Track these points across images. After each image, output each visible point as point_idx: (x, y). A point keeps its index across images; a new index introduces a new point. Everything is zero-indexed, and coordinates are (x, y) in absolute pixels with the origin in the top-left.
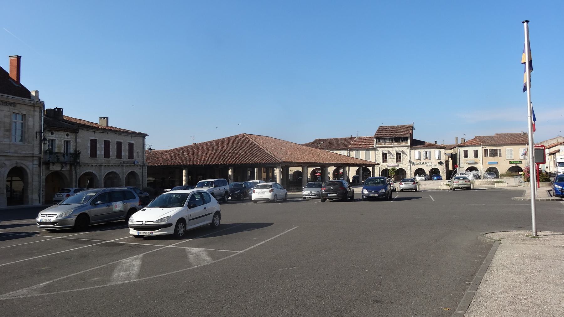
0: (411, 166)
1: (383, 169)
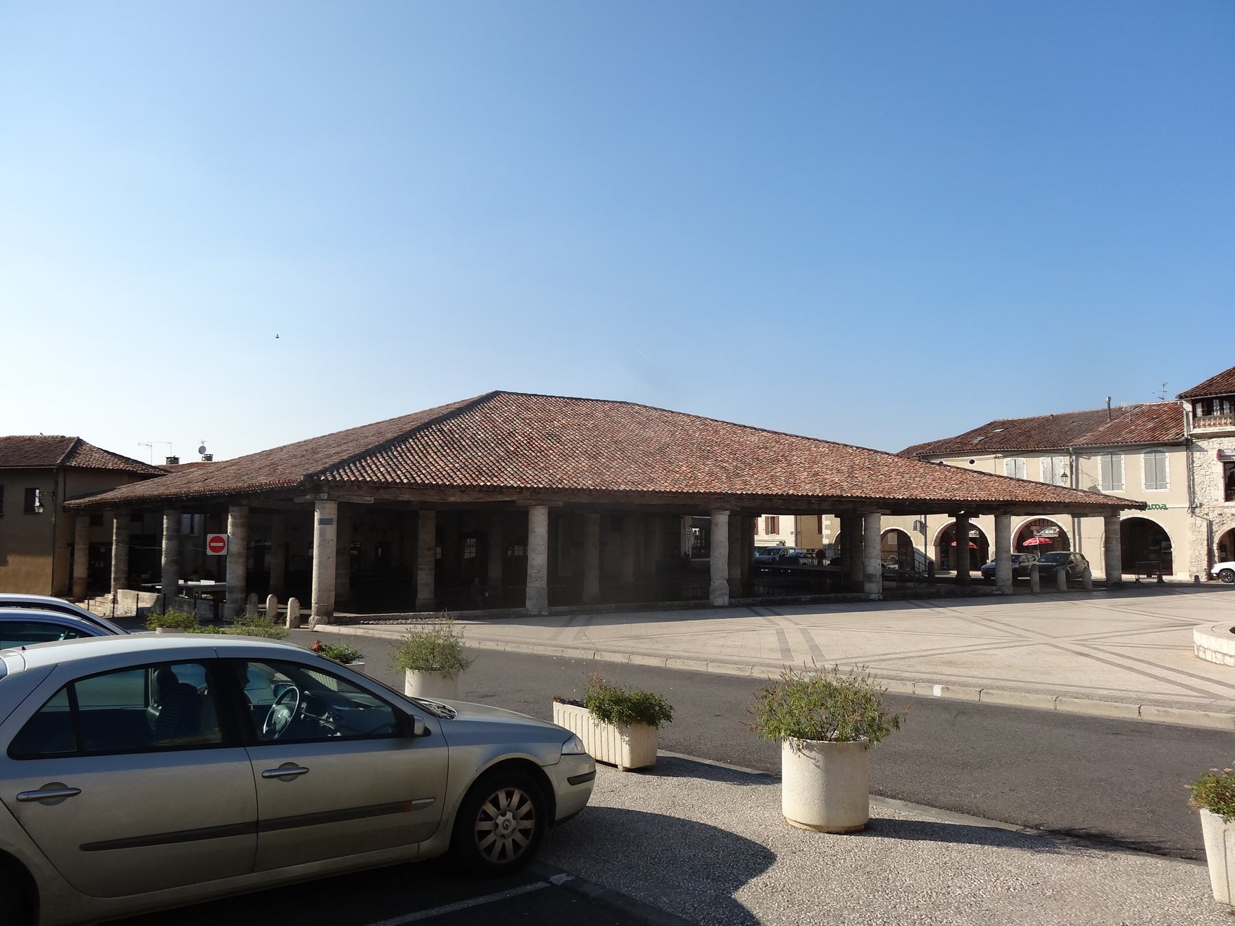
1: (1226, 528)
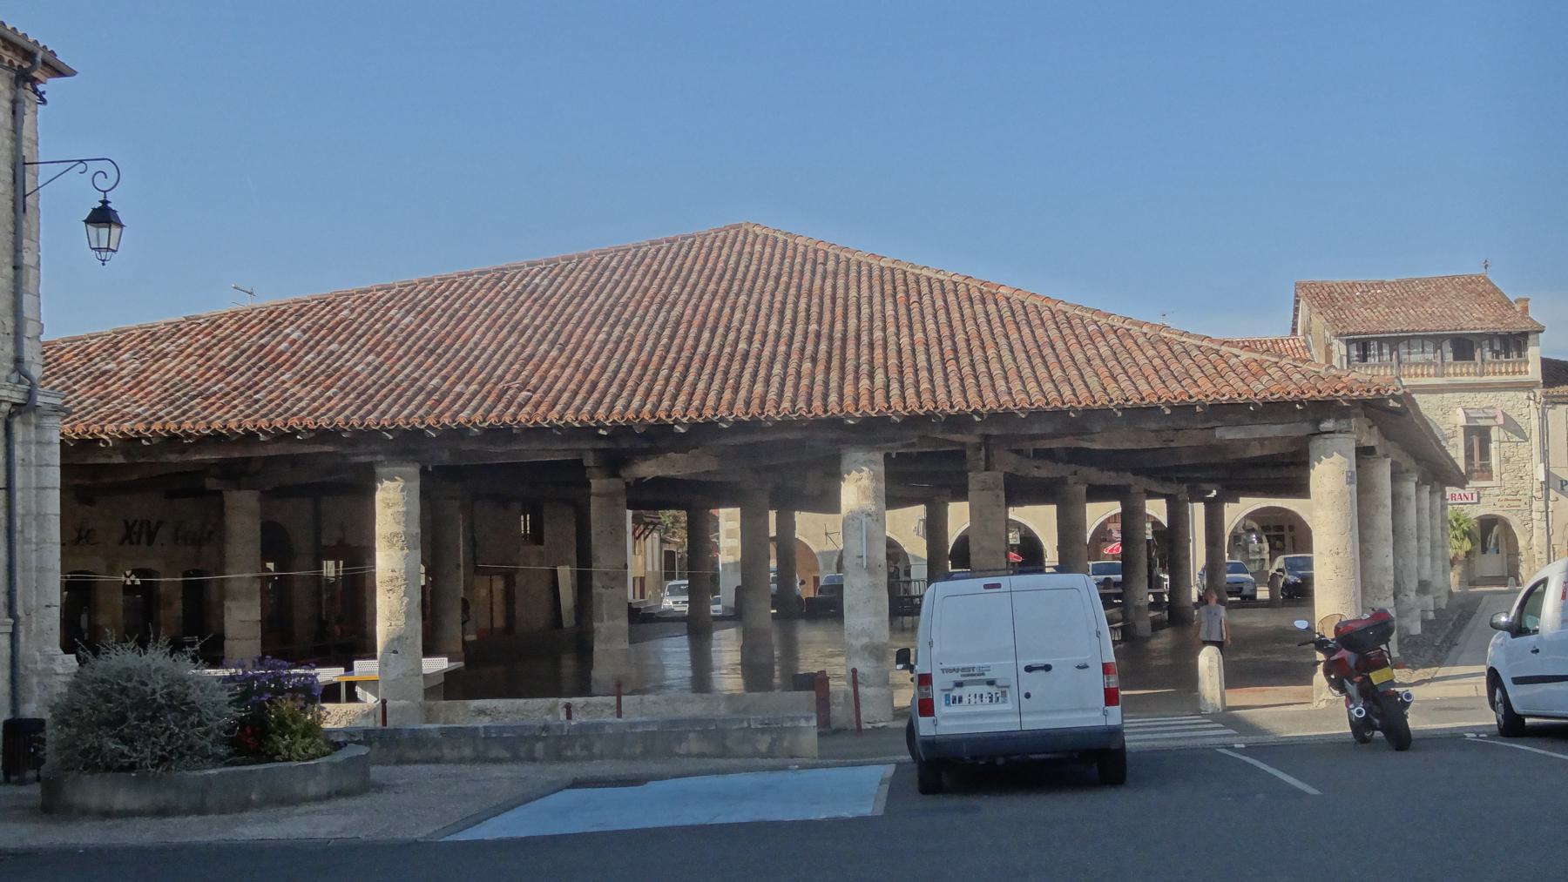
0: (1547, 498)
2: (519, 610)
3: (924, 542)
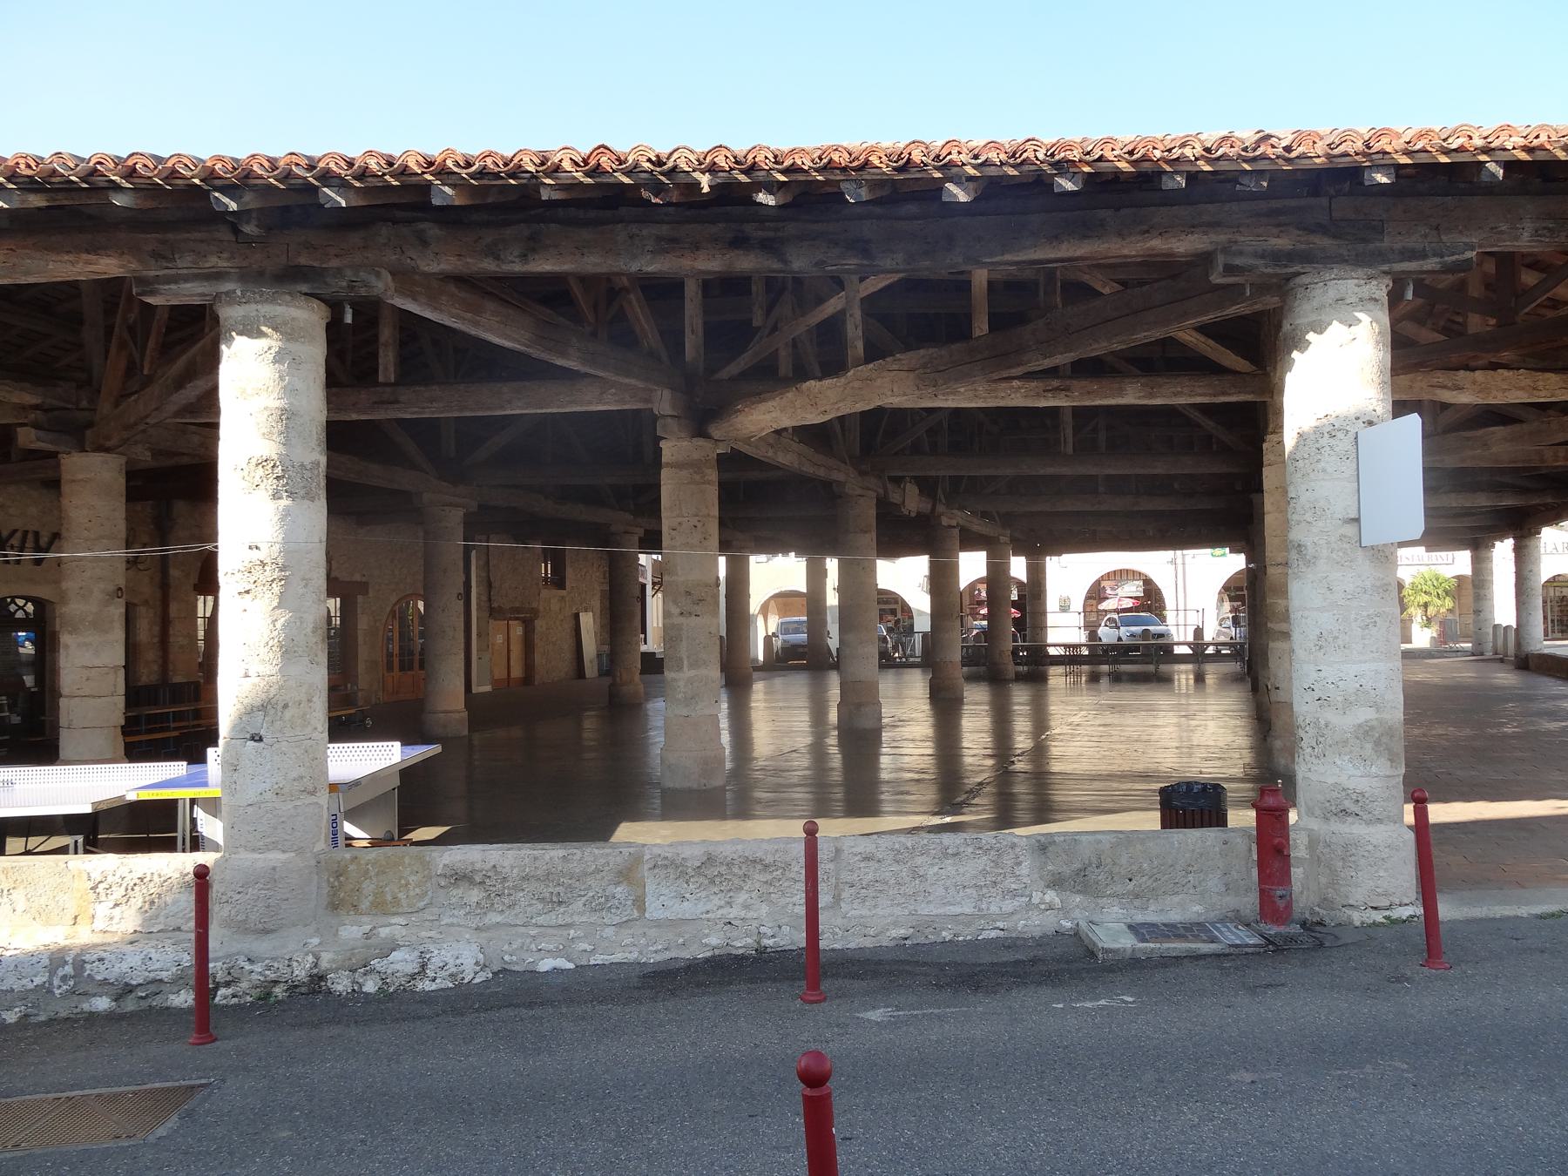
2: (538, 659)
3: (928, 597)
